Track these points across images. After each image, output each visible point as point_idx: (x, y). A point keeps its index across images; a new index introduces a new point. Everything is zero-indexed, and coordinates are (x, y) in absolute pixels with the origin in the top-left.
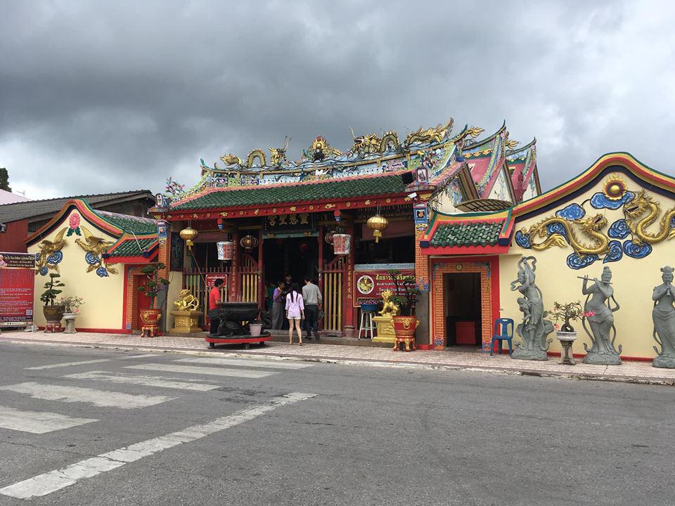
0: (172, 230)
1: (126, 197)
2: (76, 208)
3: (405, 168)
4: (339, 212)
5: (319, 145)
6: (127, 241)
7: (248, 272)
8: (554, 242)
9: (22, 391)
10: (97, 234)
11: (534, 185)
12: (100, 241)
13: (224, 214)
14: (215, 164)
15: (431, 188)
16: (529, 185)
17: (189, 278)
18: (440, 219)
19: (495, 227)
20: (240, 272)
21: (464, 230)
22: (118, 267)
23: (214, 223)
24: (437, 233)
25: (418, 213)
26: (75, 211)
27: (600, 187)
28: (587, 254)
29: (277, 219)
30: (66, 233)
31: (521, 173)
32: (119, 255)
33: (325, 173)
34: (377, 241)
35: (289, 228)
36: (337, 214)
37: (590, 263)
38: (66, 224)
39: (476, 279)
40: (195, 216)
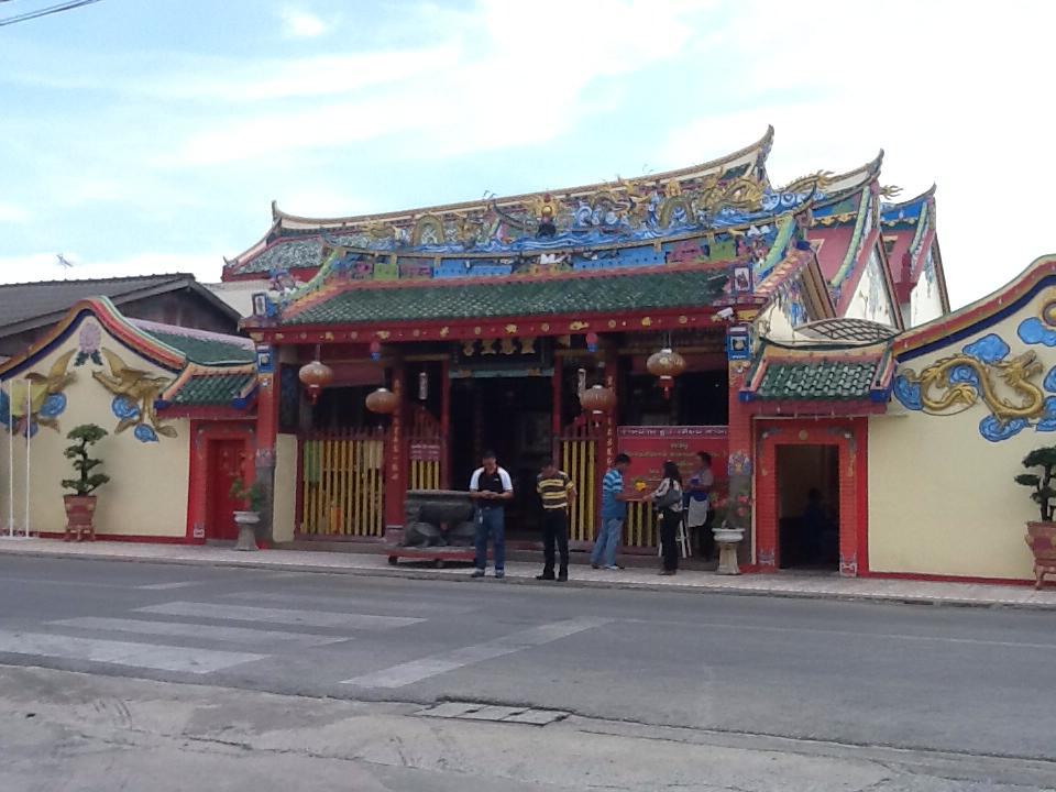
0: (282, 360)
1: (160, 285)
2: (94, 315)
3: (705, 257)
4: (595, 336)
5: (548, 209)
6: (194, 377)
7: (575, 437)
8: (960, 397)
9: (155, 611)
10: (133, 361)
11: (933, 272)
12: (139, 375)
13: (384, 335)
14: (273, 204)
15: (758, 301)
16: (923, 274)
17: (333, 445)
18: (769, 352)
19: (863, 369)
20: (408, 438)
21: (812, 372)
22: (181, 425)
23: (362, 349)
24: (767, 378)
25: (735, 342)
26: (89, 320)
27: (1032, 309)
28: (1011, 417)
29: (478, 344)
30: (73, 360)
31: (909, 251)
32: (186, 403)
33: (559, 260)
34: (655, 386)
35: (499, 359)
36: (592, 339)
37: (1014, 432)
38: (73, 343)
39: (832, 459)
40: (329, 335)
